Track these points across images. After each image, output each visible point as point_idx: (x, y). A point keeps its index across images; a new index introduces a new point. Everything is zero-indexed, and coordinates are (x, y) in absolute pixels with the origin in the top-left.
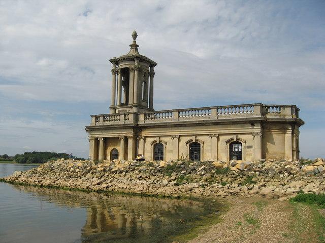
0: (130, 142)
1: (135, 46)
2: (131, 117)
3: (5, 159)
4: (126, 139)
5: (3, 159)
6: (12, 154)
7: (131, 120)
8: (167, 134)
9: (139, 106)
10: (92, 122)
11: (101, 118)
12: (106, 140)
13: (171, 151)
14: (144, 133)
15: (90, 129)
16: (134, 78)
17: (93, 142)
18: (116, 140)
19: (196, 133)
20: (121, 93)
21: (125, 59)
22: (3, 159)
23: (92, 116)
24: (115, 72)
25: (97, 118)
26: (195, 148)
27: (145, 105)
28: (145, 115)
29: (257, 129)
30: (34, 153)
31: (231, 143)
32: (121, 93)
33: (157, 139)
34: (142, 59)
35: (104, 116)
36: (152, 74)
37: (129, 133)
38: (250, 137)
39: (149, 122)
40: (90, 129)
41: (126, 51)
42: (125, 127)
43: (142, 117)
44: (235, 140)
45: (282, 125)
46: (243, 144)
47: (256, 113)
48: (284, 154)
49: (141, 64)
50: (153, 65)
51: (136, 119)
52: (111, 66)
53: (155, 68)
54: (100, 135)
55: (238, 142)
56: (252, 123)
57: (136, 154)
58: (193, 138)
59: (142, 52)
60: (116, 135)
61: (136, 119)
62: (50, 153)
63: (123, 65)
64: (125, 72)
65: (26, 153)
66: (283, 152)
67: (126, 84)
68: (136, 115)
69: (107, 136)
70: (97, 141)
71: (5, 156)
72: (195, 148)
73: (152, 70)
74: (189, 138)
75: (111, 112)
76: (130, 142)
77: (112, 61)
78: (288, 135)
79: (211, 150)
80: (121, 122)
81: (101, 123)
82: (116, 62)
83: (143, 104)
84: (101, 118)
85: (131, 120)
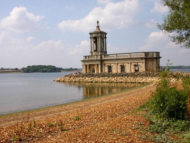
0: (99, 66)
1: (98, 27)
2: (99, 57)
3: (3, 71)
4: (98, 65)
5: (15, 71)
6: (20, 67)
7: (99, 58)
8: (113, 63)
9: (101, 51)
10: (83, 59)
11: (87, 57)
12: (90, 65)
13: (115, 69)
14: (106, 62)
15: (83, 61)
16: (99, 40)
17: (85, 66)
18: (94, 65)
19: (123, 62)
20: (94, 44)
21: (95, 33)
22: (15, 71)
23: (84, 56)
24: (91, 38)
25: (86, 57)
26: (123, 67)
27: (104, 52)
28: (104, 55)
29: (144, 61)
30: (33, 66)
31: (135, 66)
32: (94, 44)
33: (109, 65)
34: (102, 33)
35: (89, 56)
36: (106, 38)
37: (99, 63)
38: (142, 63)
39: (106, 58)
40: (83, 61)
41: (94, 29)
42: (97, 60)
43: (103, 56)
44: (136, 65)
45: (152, 59)
46: (139, 66)
47: (144, 56)
48: (153, 69)
49: (101, 34)
50: (106, 34)
51: (101, 57)
52: (90, 36)
53: (107, 35)
54: (88, 64)
55: (137, 65)
56: (142, 59)
57: (102, 71)
58: (122, 64)
59: (102, 30)
60: (94, 63)
61: (101, 57)
62: (42, 66)
63: (94, 35)
64: (95, 38)
65: (28, 67)
66: (153, 68)
67: (96, 42)
68: (101, 56)
69: (90, 64)
70: (86, 66)
71: (17, 69)
72: (123, 67)
73: (105, 36)
74: (121, 64)
75: (90, 54)
76: (99, 66)
77: (89, 34)
78: (155, 62)
79: (129, 68)
80: (95, 59)
81: (87, 59)
82: (91, 34)
83: (103, 50)
84: (87, 57)
85: (99, 58)
